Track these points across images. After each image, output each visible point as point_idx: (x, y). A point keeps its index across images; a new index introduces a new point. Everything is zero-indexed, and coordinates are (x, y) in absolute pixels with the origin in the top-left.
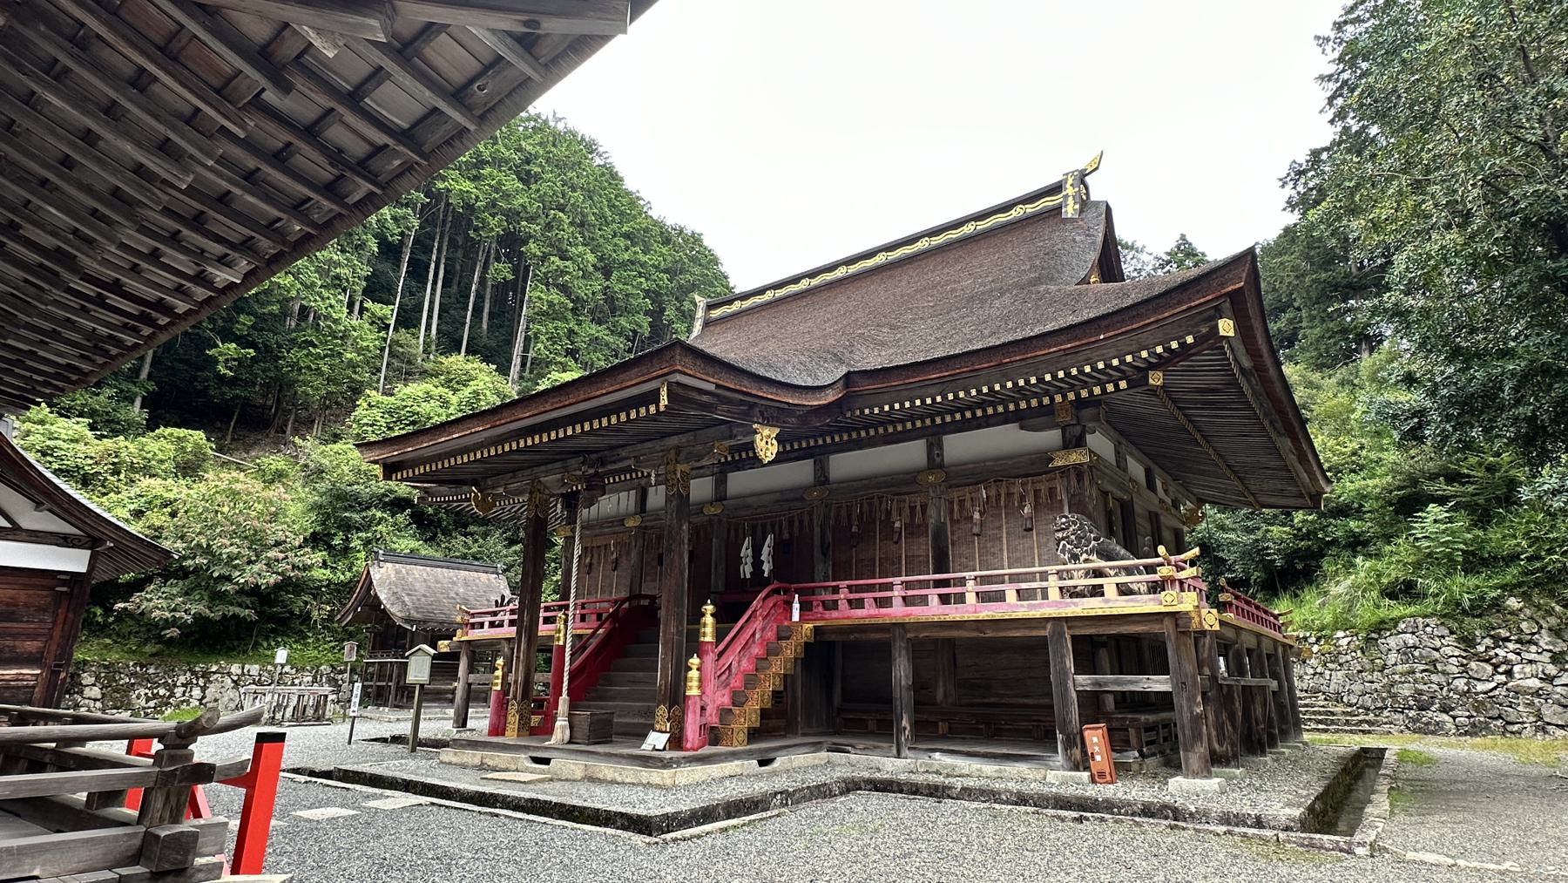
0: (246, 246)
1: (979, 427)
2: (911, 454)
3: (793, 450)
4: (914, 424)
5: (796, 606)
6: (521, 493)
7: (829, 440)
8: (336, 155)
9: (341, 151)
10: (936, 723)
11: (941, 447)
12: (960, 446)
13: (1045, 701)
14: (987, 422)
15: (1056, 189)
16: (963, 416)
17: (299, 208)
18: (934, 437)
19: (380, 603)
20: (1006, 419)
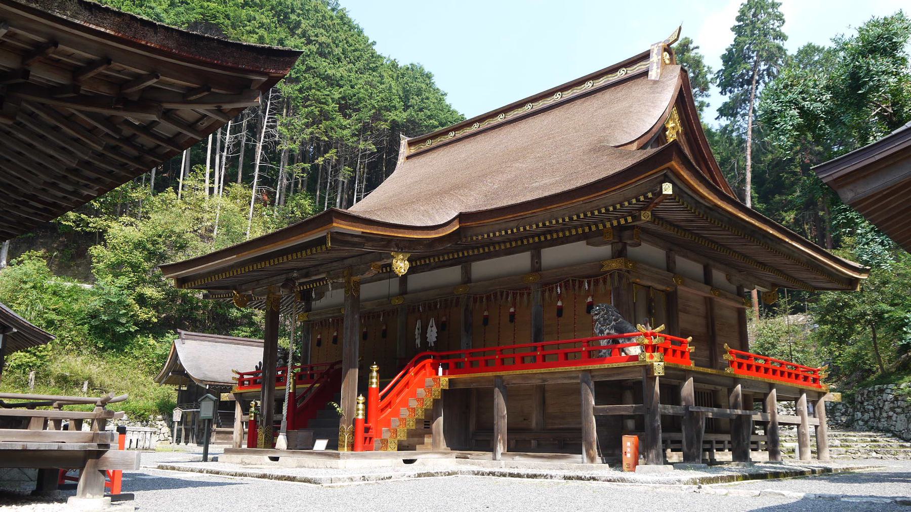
0: (97, 181)
1: (562, 243)
2: (521, 261)
3: (444, 261)
4: (511, 244)
5: (440, 370)
6: (263, 295)
7: (461, 255)
8: (140, 148)
9: (142, 145)
10: (530, 441)
11: (539, 257)
12: (552, 256)
13: (578, 426)
14: (497, 254)
15: (646, 56)
16: (539, 239)
17: (123, 166)
18: (536, 250)
19: (184, 370)
20: (578, 238)
